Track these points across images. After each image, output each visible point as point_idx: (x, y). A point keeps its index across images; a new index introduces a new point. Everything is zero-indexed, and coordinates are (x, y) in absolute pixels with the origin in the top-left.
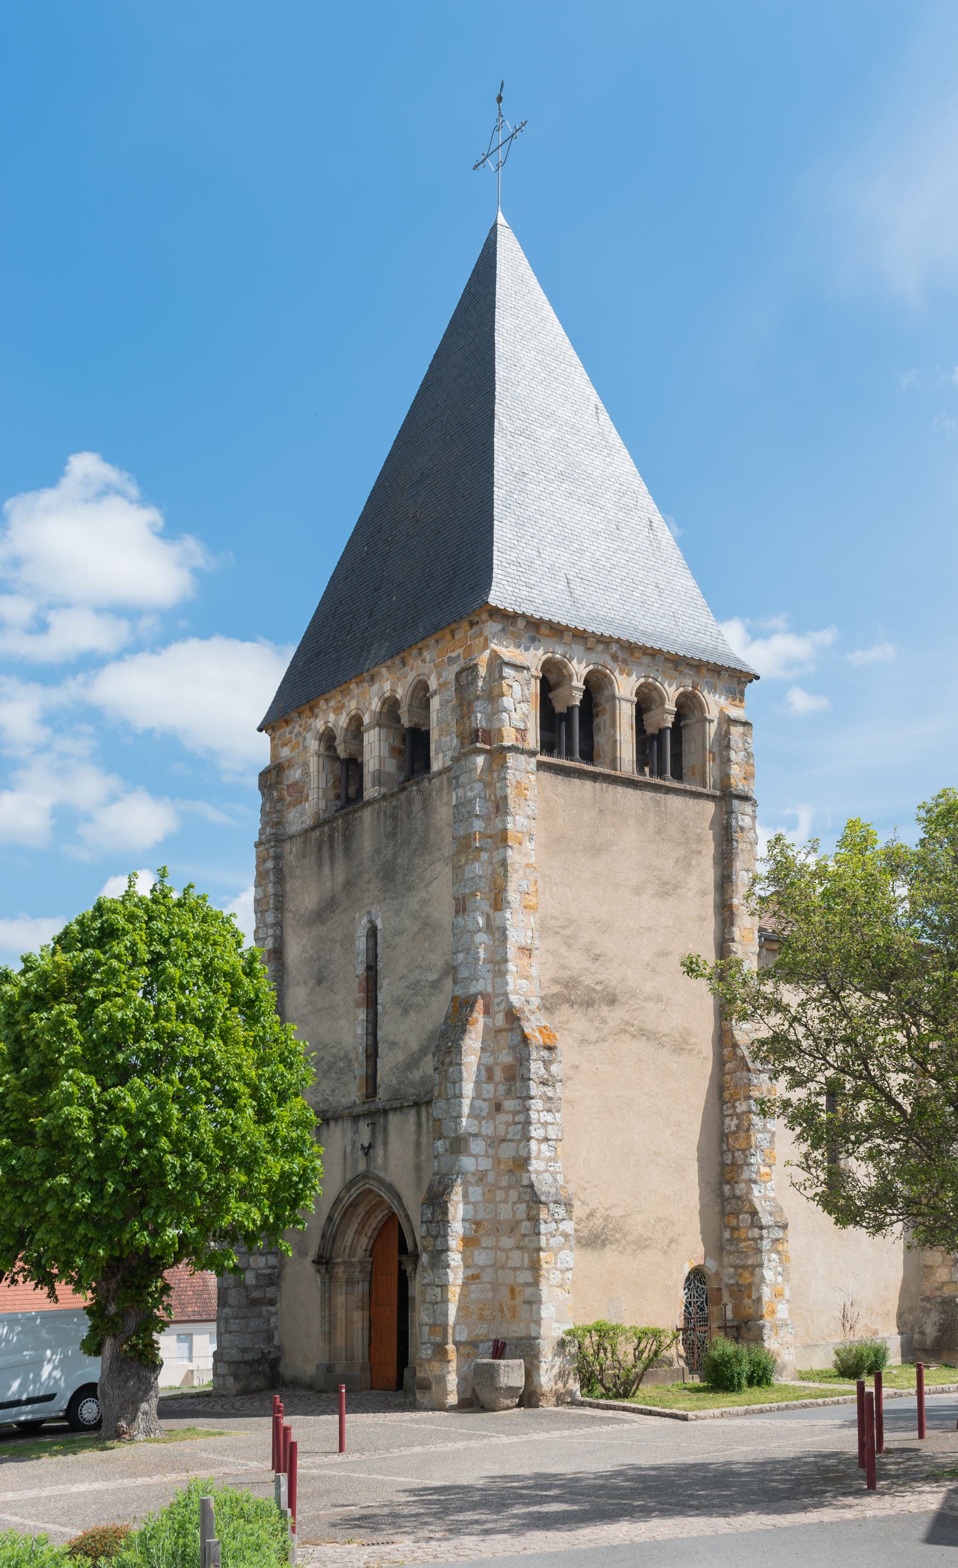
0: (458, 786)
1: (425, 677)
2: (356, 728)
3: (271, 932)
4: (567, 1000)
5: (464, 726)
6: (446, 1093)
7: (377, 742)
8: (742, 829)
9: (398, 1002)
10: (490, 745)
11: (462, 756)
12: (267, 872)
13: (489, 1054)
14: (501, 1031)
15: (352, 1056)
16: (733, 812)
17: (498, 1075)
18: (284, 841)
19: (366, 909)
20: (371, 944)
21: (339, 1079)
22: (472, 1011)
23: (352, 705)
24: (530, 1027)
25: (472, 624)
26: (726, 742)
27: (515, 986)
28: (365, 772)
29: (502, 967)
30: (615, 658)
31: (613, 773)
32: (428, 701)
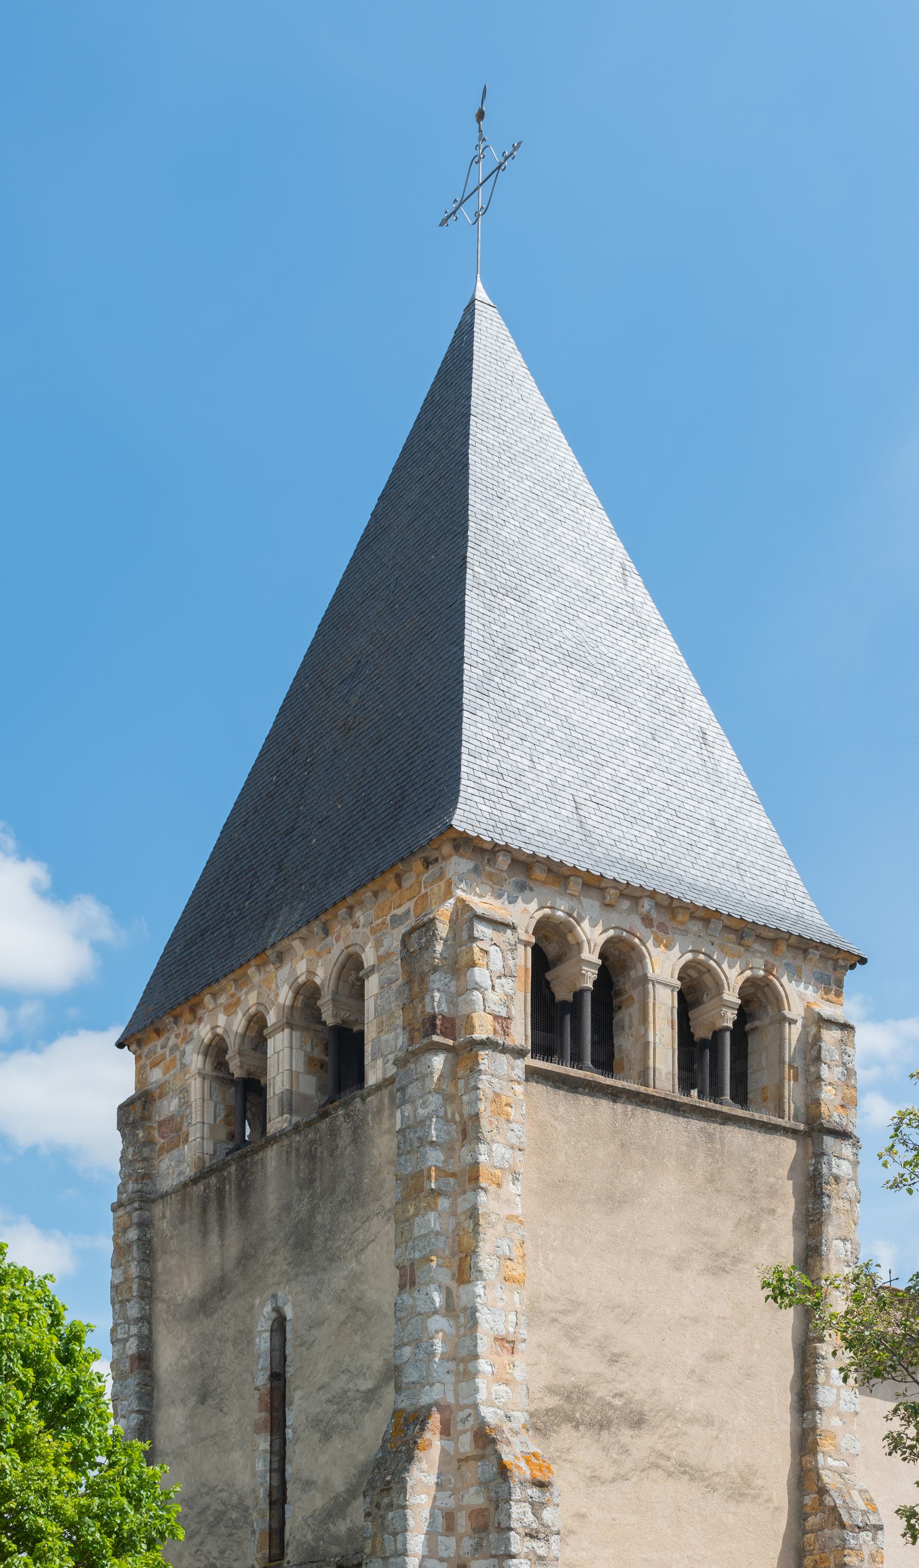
0: (404, 1102)
1: (357, 949)
2: (257, 1033)
3: (134, 1330)
4: (569, 1419)
5: (415, 1013)
6: (383, 1550)
7: (287, 1051)
8: (837, 1179)
9: (315, 1423)
10: (454, 1039)
11: (408, 1059)
12: (129, 1246)
13: (448, 1493)
14: (467, 1459)
15: (249, 1502)
16: (823, 1154)
17: (463, 1523)
18: (153, 1201)
19: (269, 1293)
20: (277, 1343)
21: (231, 1535)
22: (422, 1430)
23: (251, 999)
24: (515, 1451)
25: (427, 863)
26: (814, 1053)
27: (490, 1393)
28: (270, 1093)
29: (470, 1366)
30: (647, 921)
31: (642, 1089)
32: (362, 981)
